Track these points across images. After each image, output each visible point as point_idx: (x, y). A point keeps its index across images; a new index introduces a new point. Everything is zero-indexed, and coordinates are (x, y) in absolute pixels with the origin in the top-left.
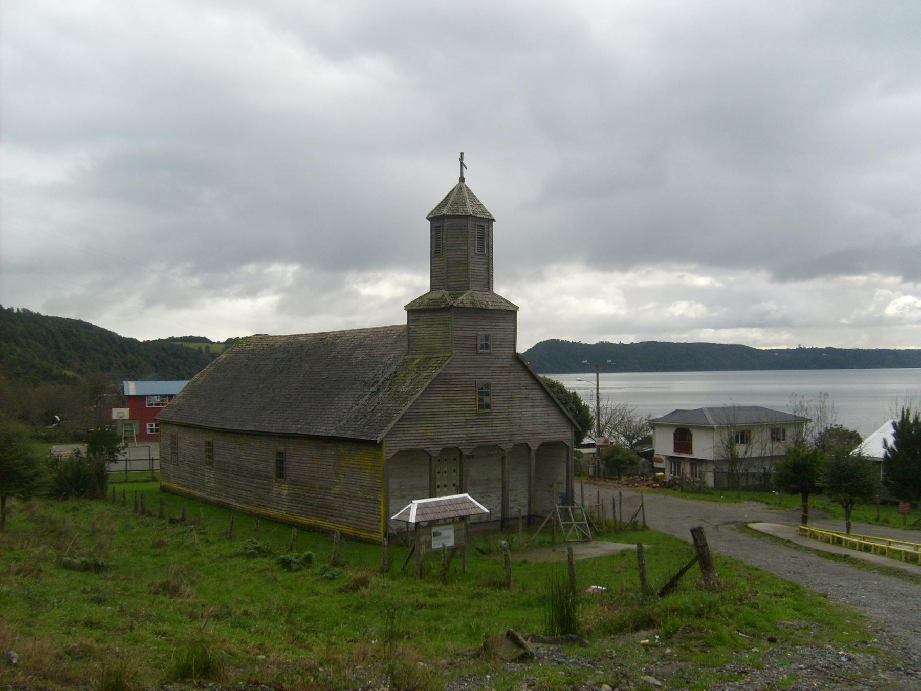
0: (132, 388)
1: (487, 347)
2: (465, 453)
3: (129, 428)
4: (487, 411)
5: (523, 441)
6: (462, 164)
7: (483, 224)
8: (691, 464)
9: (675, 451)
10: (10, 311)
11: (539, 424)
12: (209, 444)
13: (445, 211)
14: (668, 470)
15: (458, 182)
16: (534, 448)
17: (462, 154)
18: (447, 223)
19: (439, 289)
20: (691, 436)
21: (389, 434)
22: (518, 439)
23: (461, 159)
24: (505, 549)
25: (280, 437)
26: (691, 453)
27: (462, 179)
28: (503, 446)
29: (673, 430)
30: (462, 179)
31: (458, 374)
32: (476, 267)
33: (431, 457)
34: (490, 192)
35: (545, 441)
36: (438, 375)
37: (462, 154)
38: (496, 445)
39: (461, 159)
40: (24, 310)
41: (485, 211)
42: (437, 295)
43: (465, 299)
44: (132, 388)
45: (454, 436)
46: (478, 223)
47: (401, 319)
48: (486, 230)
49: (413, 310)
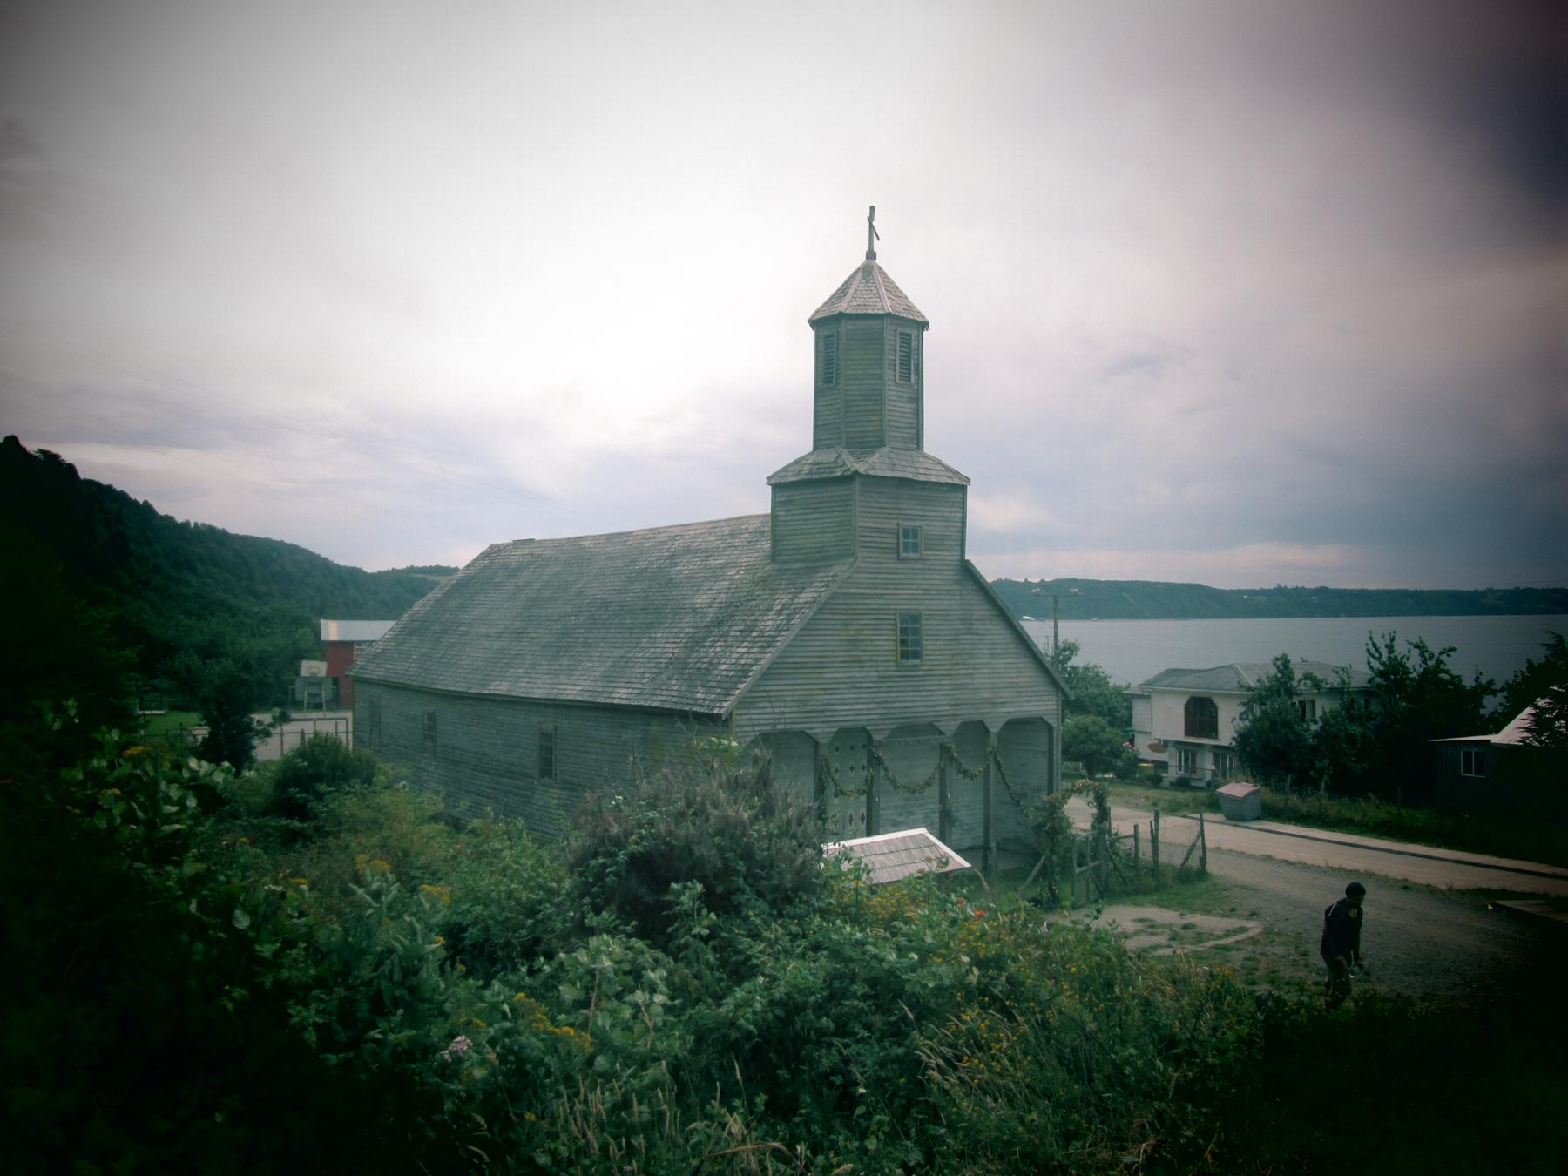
0: (332, 630)
1: (915, 548)
2: (877, 737)
3: (314, 690)
4: (917, 662)
5: (977, 717)
6: (871, 226)
7: (911, 328)
8: (1216, 756)
9: (1188, 733)
10: (169, 520)
11: (1008, 693)
12: (432, 717)
13: (843, 307)
14: (1173, 763)
15: (863, 259)
16: (994, 730)
17: (872, 209)
18: (846, 327)
19: (829, 446)
20: (1216, 708)
21: (743, 703)
22: (968, 713)
23: (871, 219)
24: (1185, 1123)
25: (546, 706)
26: (1216, 738)
27: (871, 255)
28: (942, 726)
29: (1184, 700)
30: (871, 255)
31: (863, 596)
32: (896, 407)
33: (816, 744)
34: (916, 279)
35: (1014, 716)
36: (831, 598)
37: (872, 209)
38: (931, 724)
39: (871, 219)
40: (146, 502)
41: (910, 308)
42: (828, 456)
43: (875, 464)
44: (332, 630)
45: (854, 709)
46: (900, 329)
47: (760, 503)
48: (914, 344)
49: (785, 487)
